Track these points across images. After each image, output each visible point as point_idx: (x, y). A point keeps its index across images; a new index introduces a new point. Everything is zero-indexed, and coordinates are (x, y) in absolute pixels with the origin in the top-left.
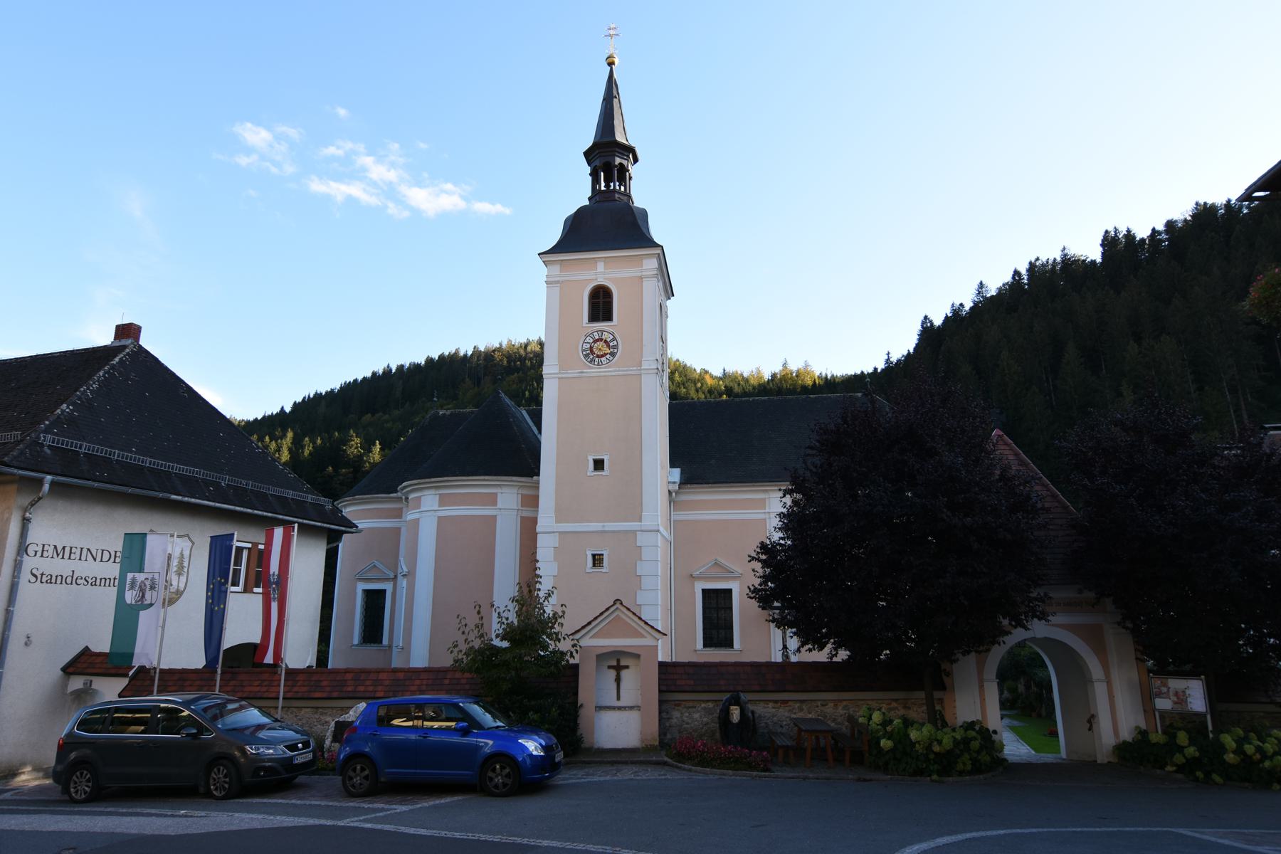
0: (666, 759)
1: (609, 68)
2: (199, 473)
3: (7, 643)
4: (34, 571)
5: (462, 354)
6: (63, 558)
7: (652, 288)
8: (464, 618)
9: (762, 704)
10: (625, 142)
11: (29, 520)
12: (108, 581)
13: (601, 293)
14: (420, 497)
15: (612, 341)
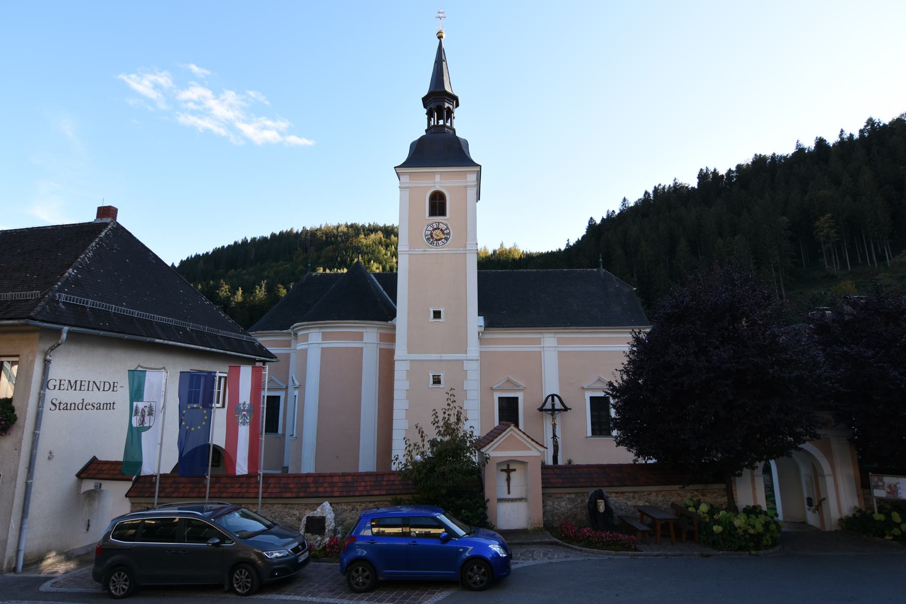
0: (556, 540)
2: (172, 321)
3: (35, 459)
4: (53, 401)
5: (295, 231)
6: (75, 390)
7: (472, 193)
8: (409, 440)
11: (49, 361)
12: (109, 405)
13: (438, 195)
14: (308, 334)
15: (446, 229)
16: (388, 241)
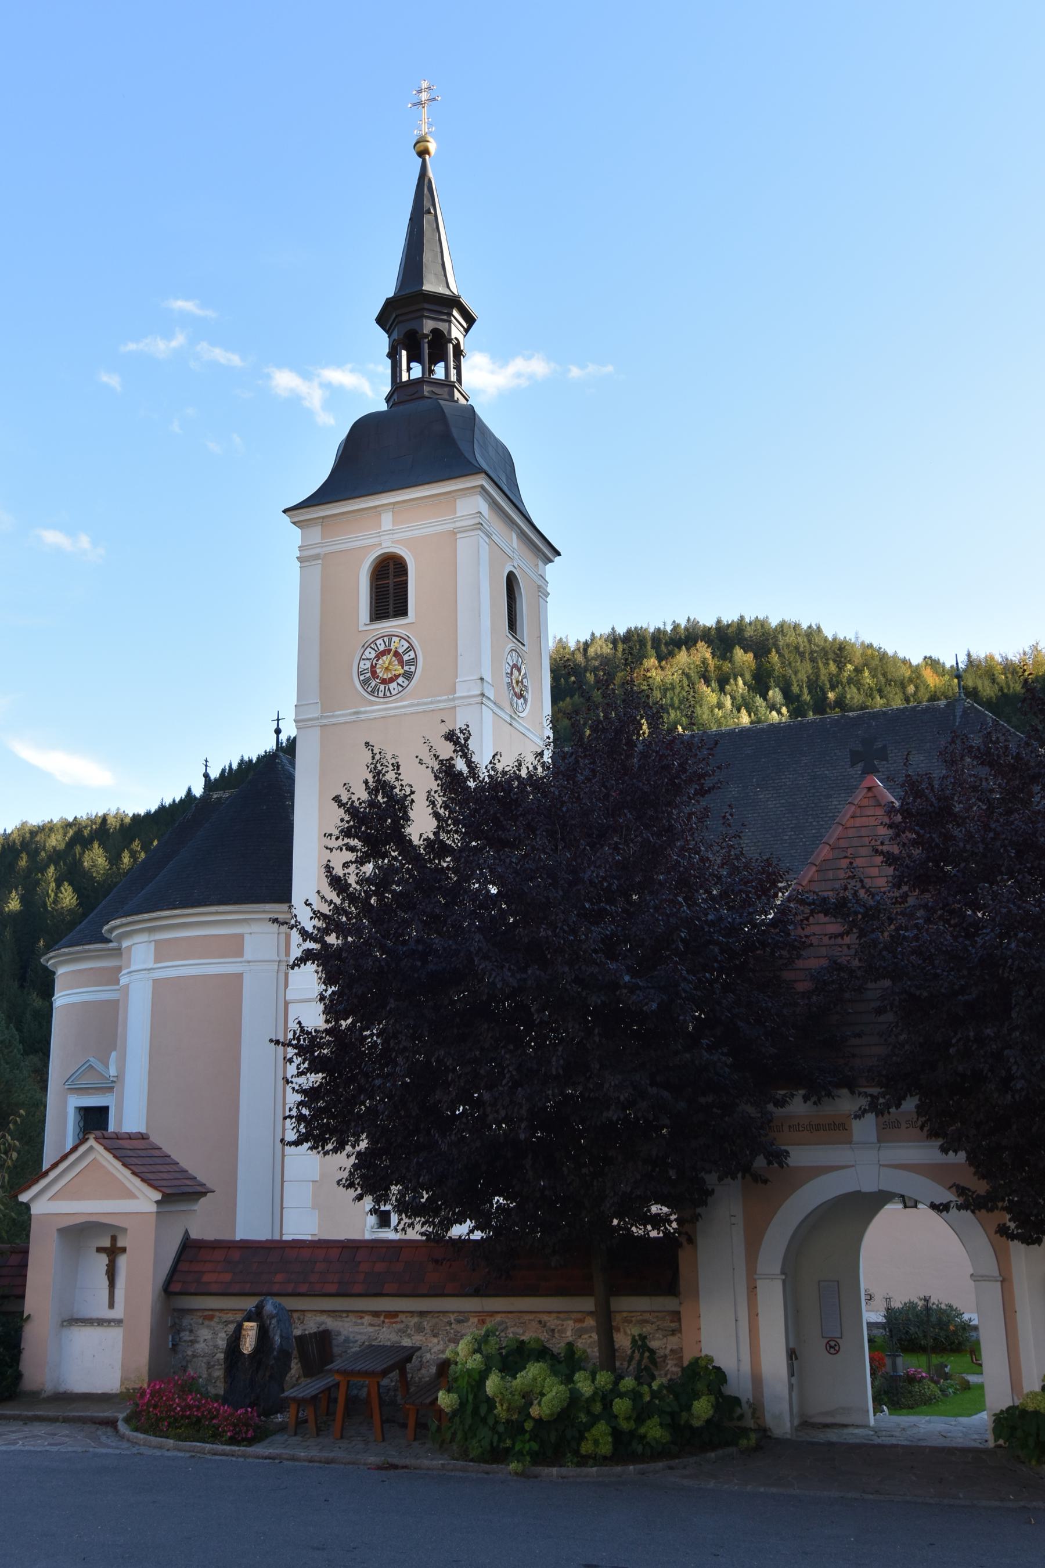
1: (421, 160)
9: (352, 1318)
10: (448, 293)
13: (392, 566)
15: (406, 652)
16: (727, 666)
